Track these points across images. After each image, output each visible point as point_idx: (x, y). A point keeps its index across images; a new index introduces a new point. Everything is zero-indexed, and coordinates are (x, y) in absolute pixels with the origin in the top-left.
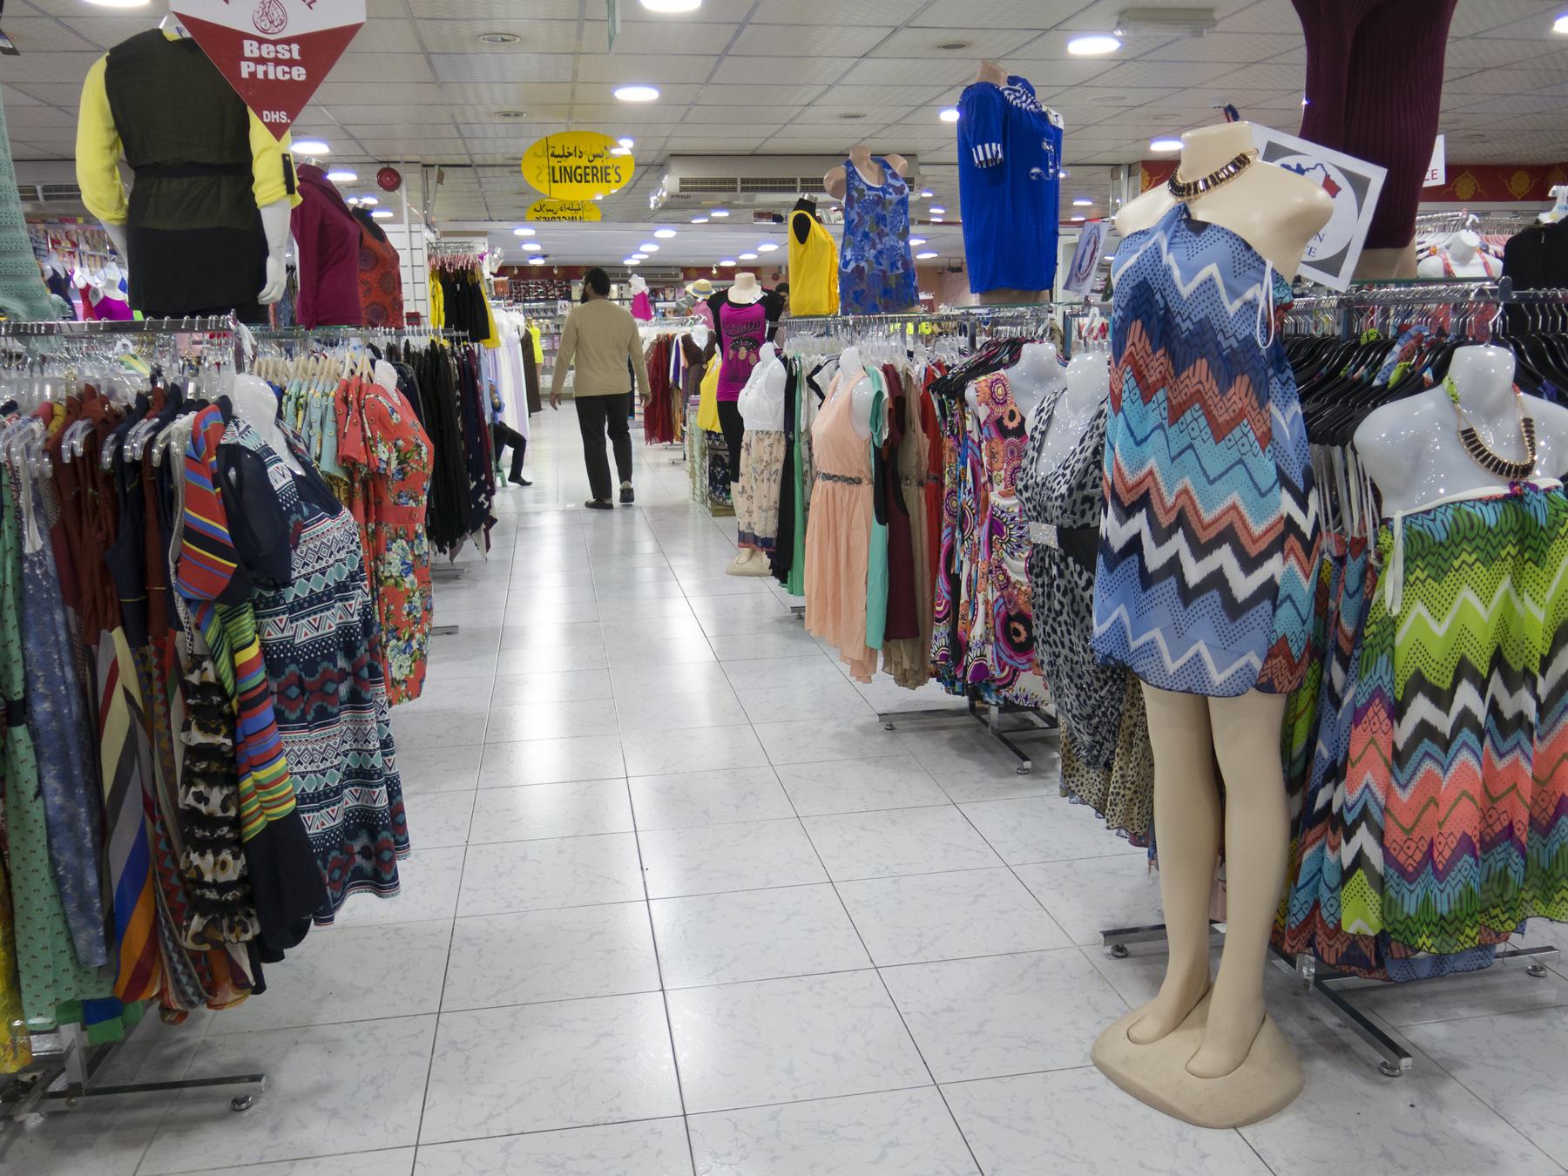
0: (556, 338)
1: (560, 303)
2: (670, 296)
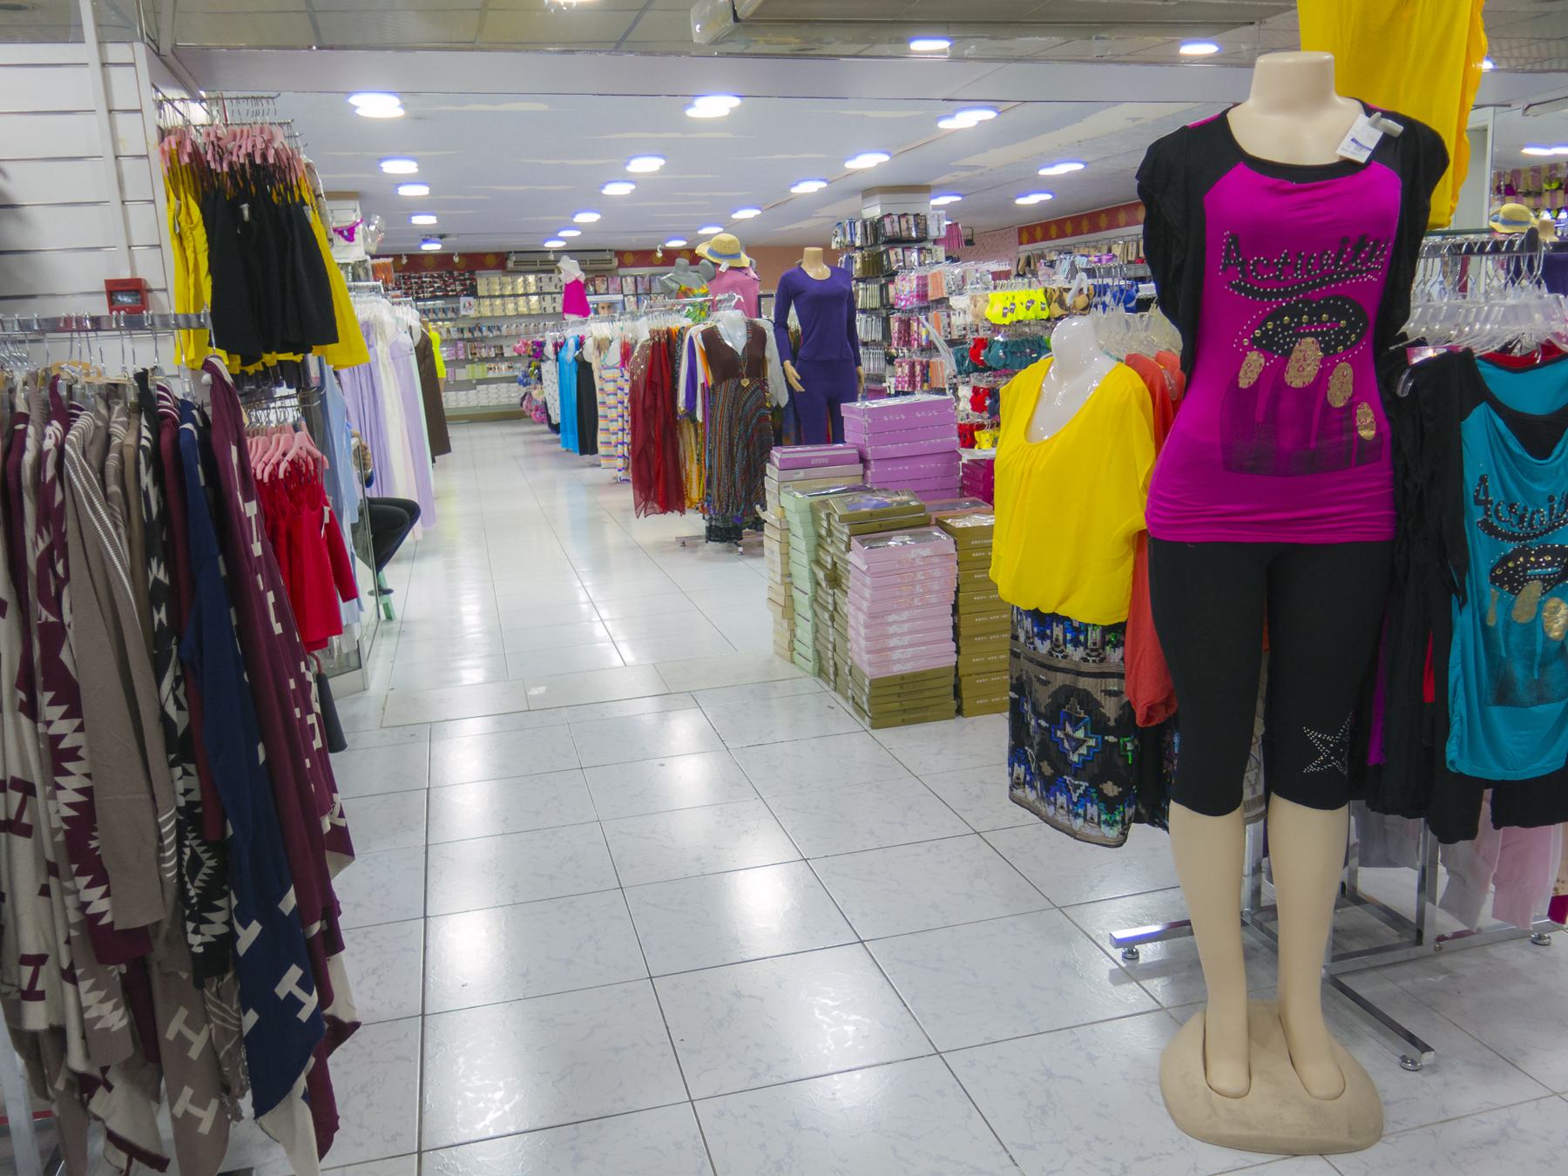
0: (460, 345)
1: (464, 300)
2: (602, 287)
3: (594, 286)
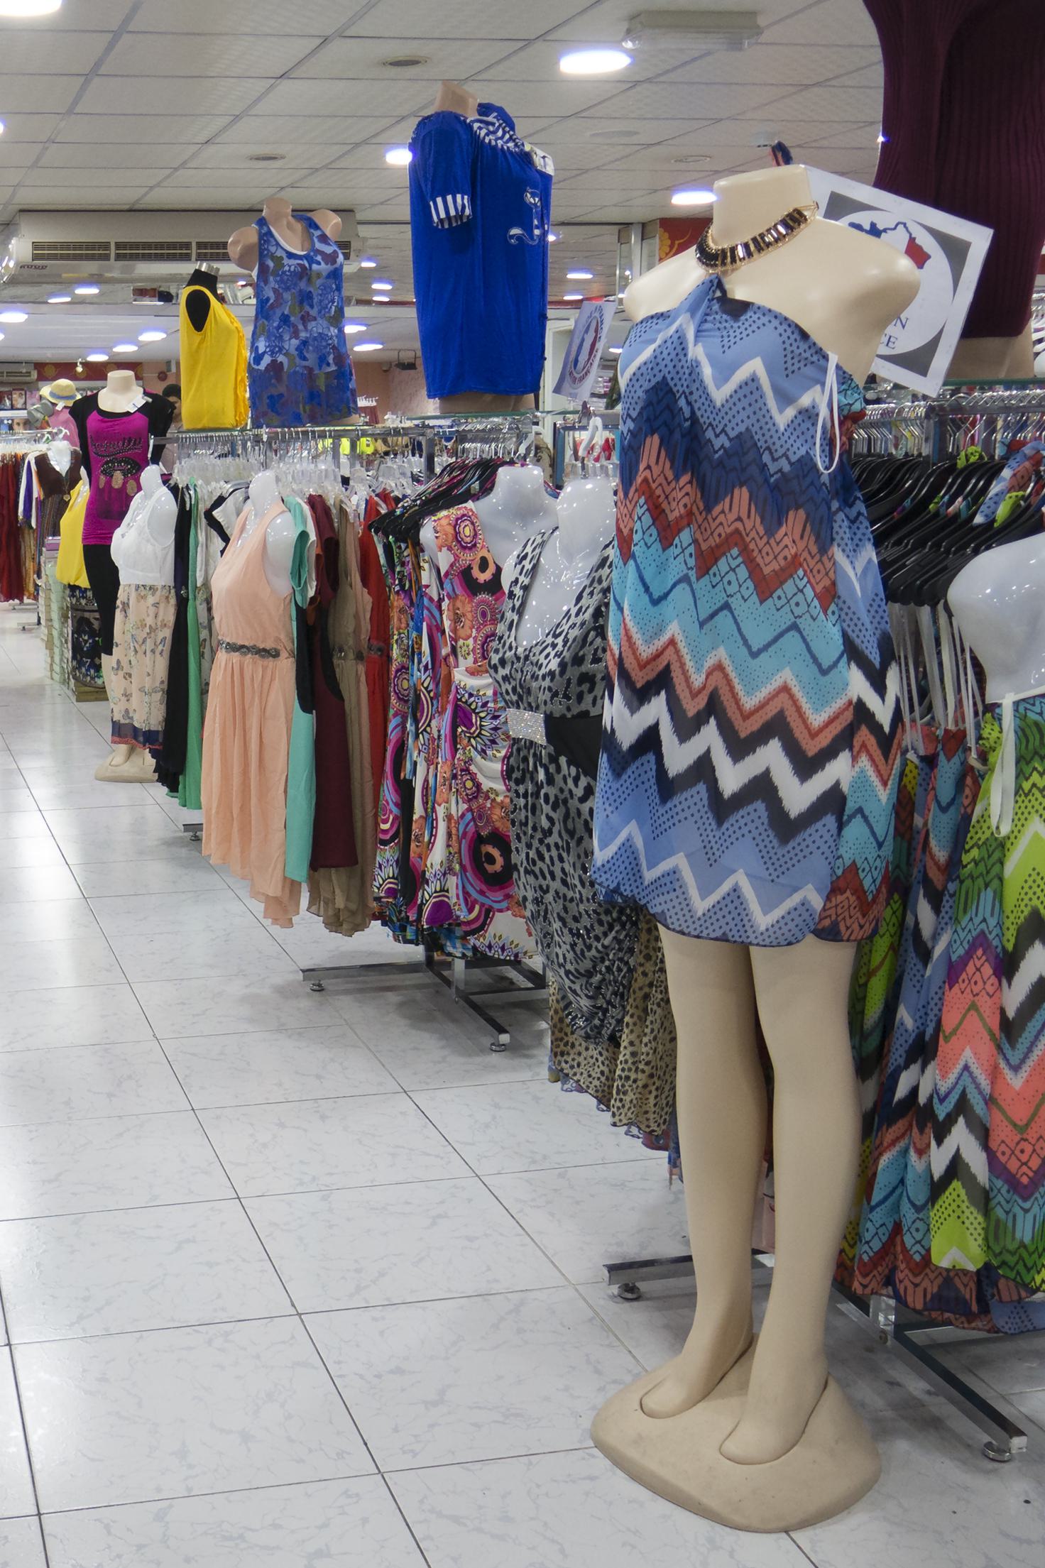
3: (11, 400)
